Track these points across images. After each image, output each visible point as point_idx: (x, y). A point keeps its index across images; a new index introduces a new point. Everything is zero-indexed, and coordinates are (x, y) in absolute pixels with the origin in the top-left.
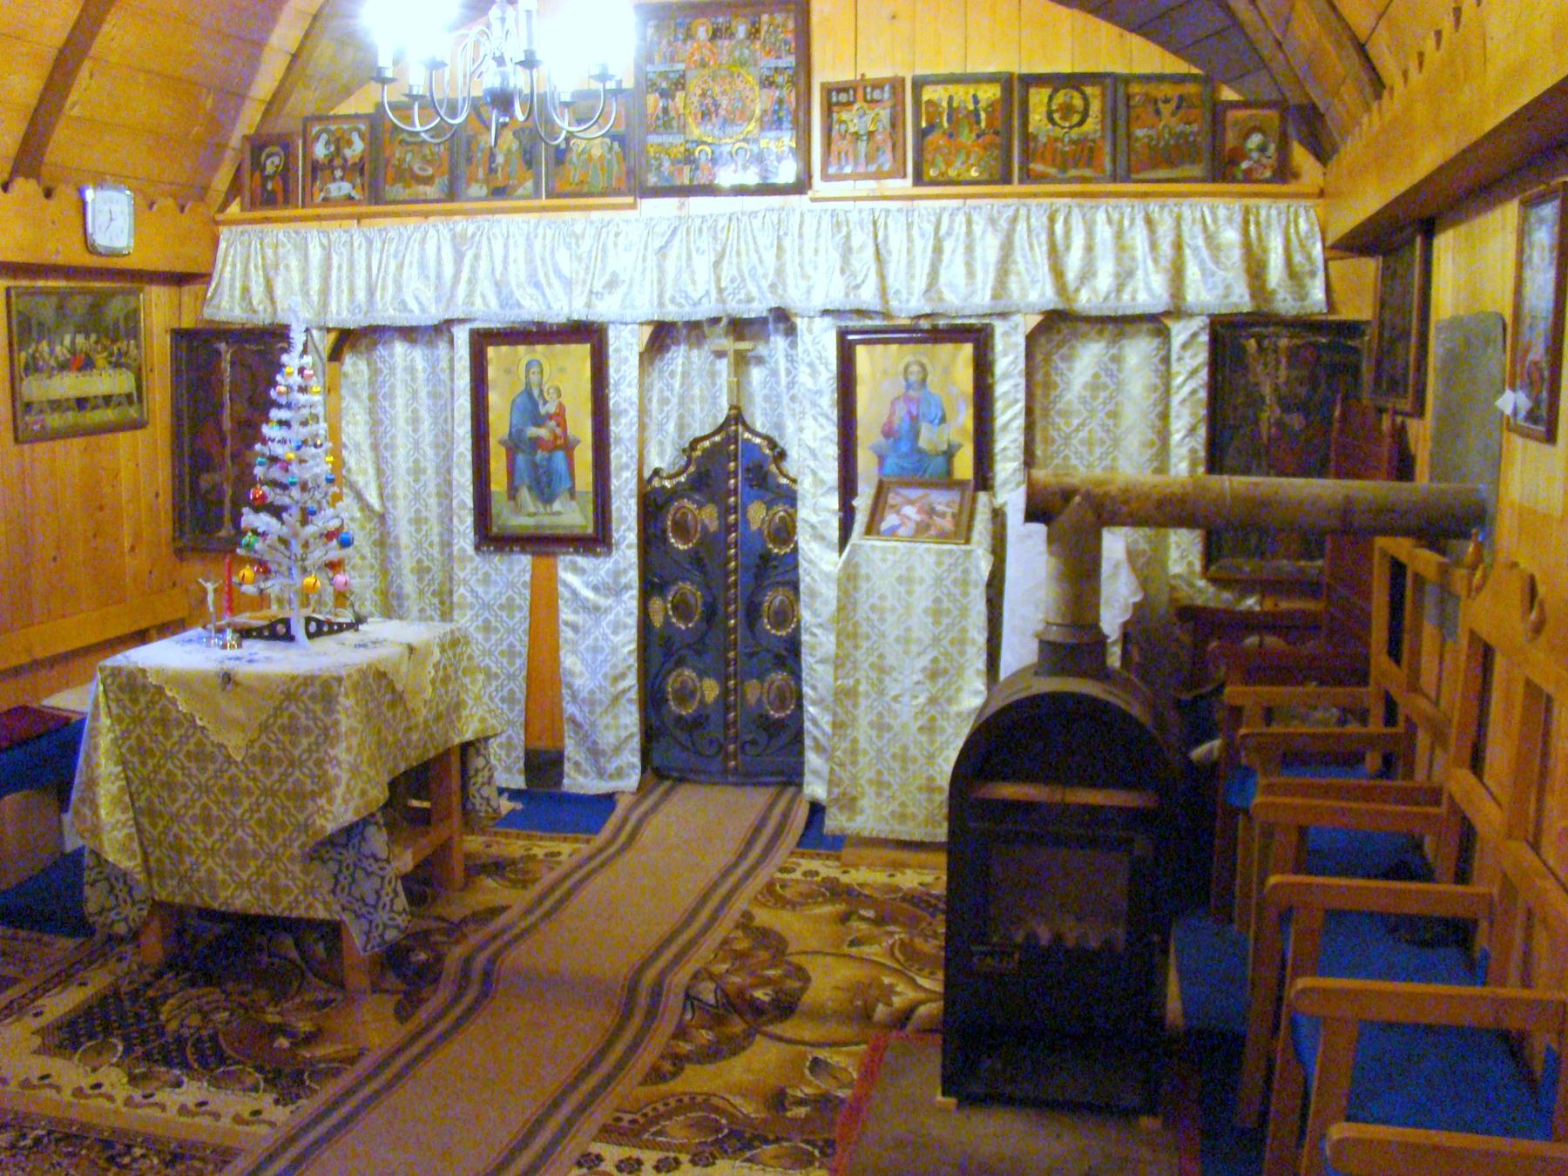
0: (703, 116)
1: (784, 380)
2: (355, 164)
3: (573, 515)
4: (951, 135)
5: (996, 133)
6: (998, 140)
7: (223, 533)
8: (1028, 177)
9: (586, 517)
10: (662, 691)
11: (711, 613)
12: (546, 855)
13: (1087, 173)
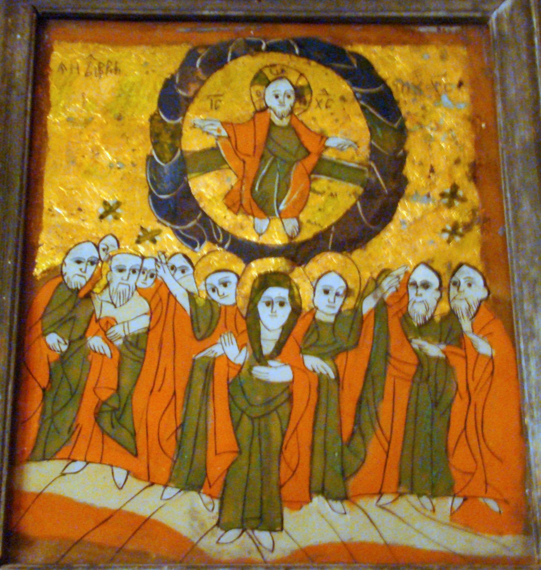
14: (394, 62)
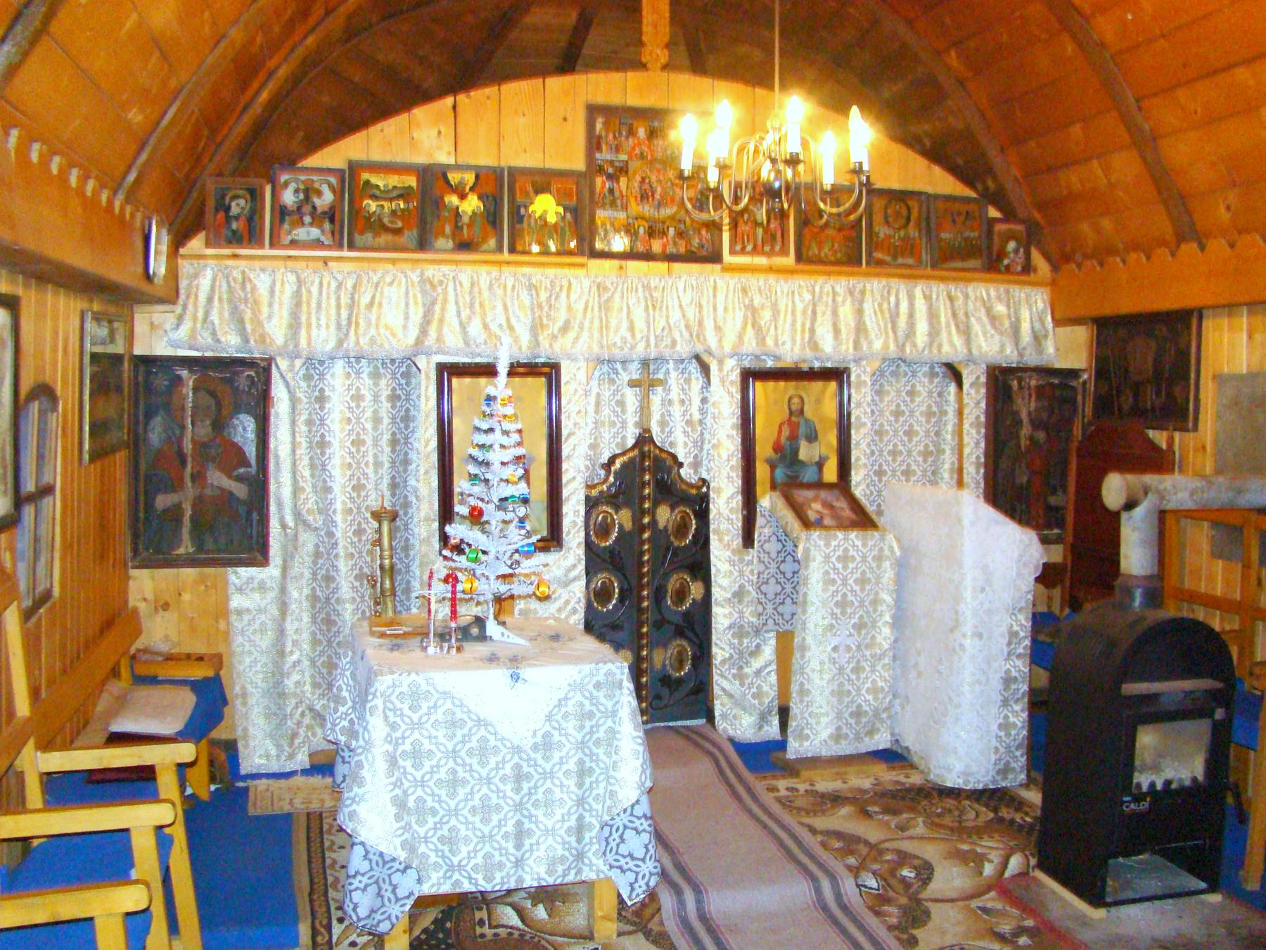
0: (642, 197)
2: (324, 213)
7: (181, 551)
13: (910, 261)
14: (910, 203)
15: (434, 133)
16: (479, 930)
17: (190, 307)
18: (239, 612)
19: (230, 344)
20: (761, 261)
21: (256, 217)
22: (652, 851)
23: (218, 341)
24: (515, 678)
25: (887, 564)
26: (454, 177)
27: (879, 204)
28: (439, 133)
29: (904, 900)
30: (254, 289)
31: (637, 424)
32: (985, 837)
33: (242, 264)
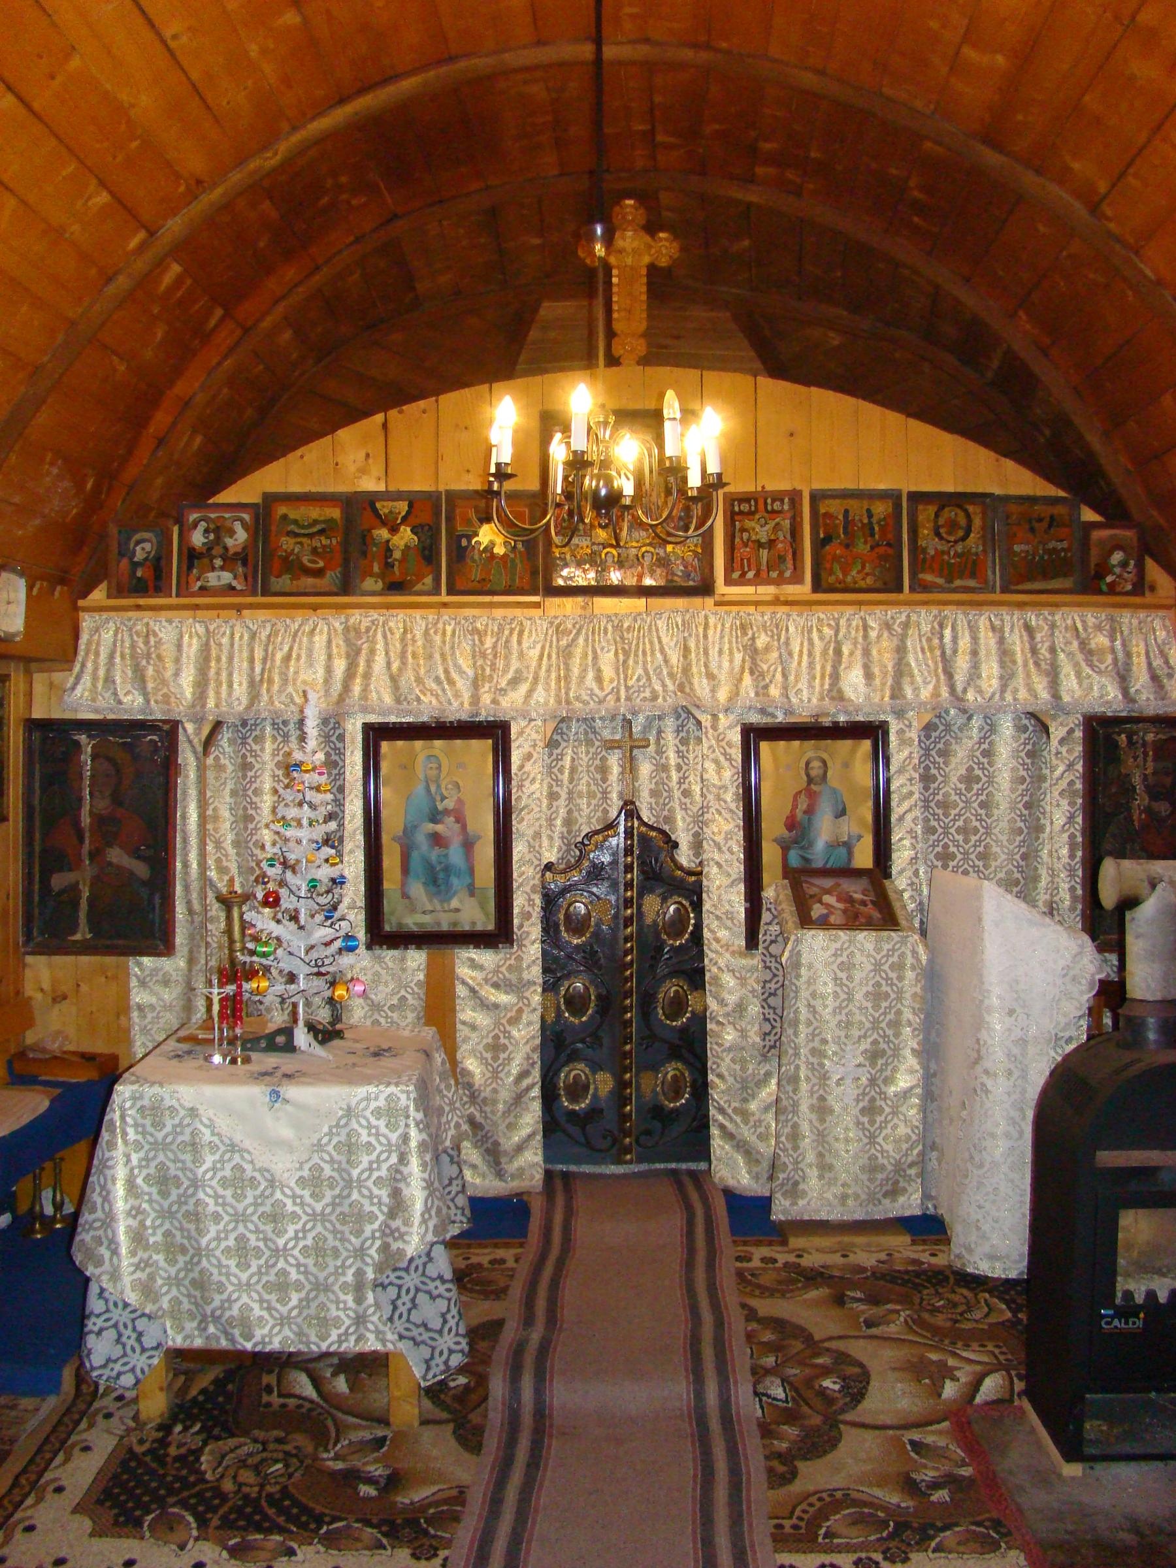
1: (675, 776)
2: (236, 554)
3: (475, 914)
4: (847, 546)
5: (889, 545)
6: (890, 551)
7: (78, 937)
8: (919, 586)
9: (487, 915)
10: (555, 1087)
11: (605, 1003)
12: (490, 1262)
13: (972, 583)
14: (971, 508)
15: (362, 455)
16: (265, 1398)
17: (89, 665)
18: (140, 1008)
19: (132, 704)
20: (767, 591)
21: (163, 562)
22: (452, 1323)
23: (120, 702)
24: (275, 1095)
25: (910, 975)
26: (383, 507)
27: (927, 513)
28: (368, 455)
29: (816, 1420)
30: (159, 642)
31: (621, 795)
32: (975, 1346)
33: (147, 616)
